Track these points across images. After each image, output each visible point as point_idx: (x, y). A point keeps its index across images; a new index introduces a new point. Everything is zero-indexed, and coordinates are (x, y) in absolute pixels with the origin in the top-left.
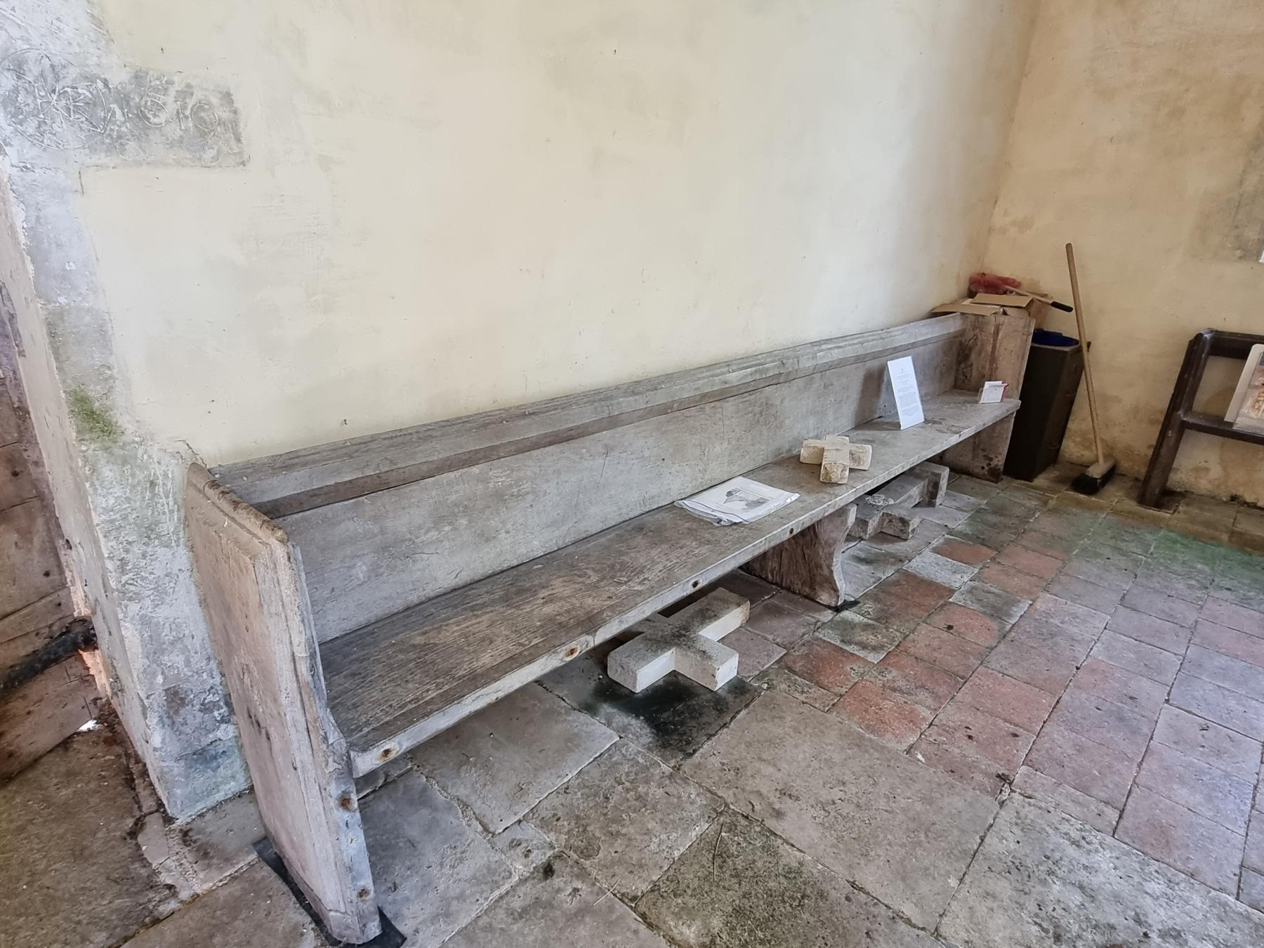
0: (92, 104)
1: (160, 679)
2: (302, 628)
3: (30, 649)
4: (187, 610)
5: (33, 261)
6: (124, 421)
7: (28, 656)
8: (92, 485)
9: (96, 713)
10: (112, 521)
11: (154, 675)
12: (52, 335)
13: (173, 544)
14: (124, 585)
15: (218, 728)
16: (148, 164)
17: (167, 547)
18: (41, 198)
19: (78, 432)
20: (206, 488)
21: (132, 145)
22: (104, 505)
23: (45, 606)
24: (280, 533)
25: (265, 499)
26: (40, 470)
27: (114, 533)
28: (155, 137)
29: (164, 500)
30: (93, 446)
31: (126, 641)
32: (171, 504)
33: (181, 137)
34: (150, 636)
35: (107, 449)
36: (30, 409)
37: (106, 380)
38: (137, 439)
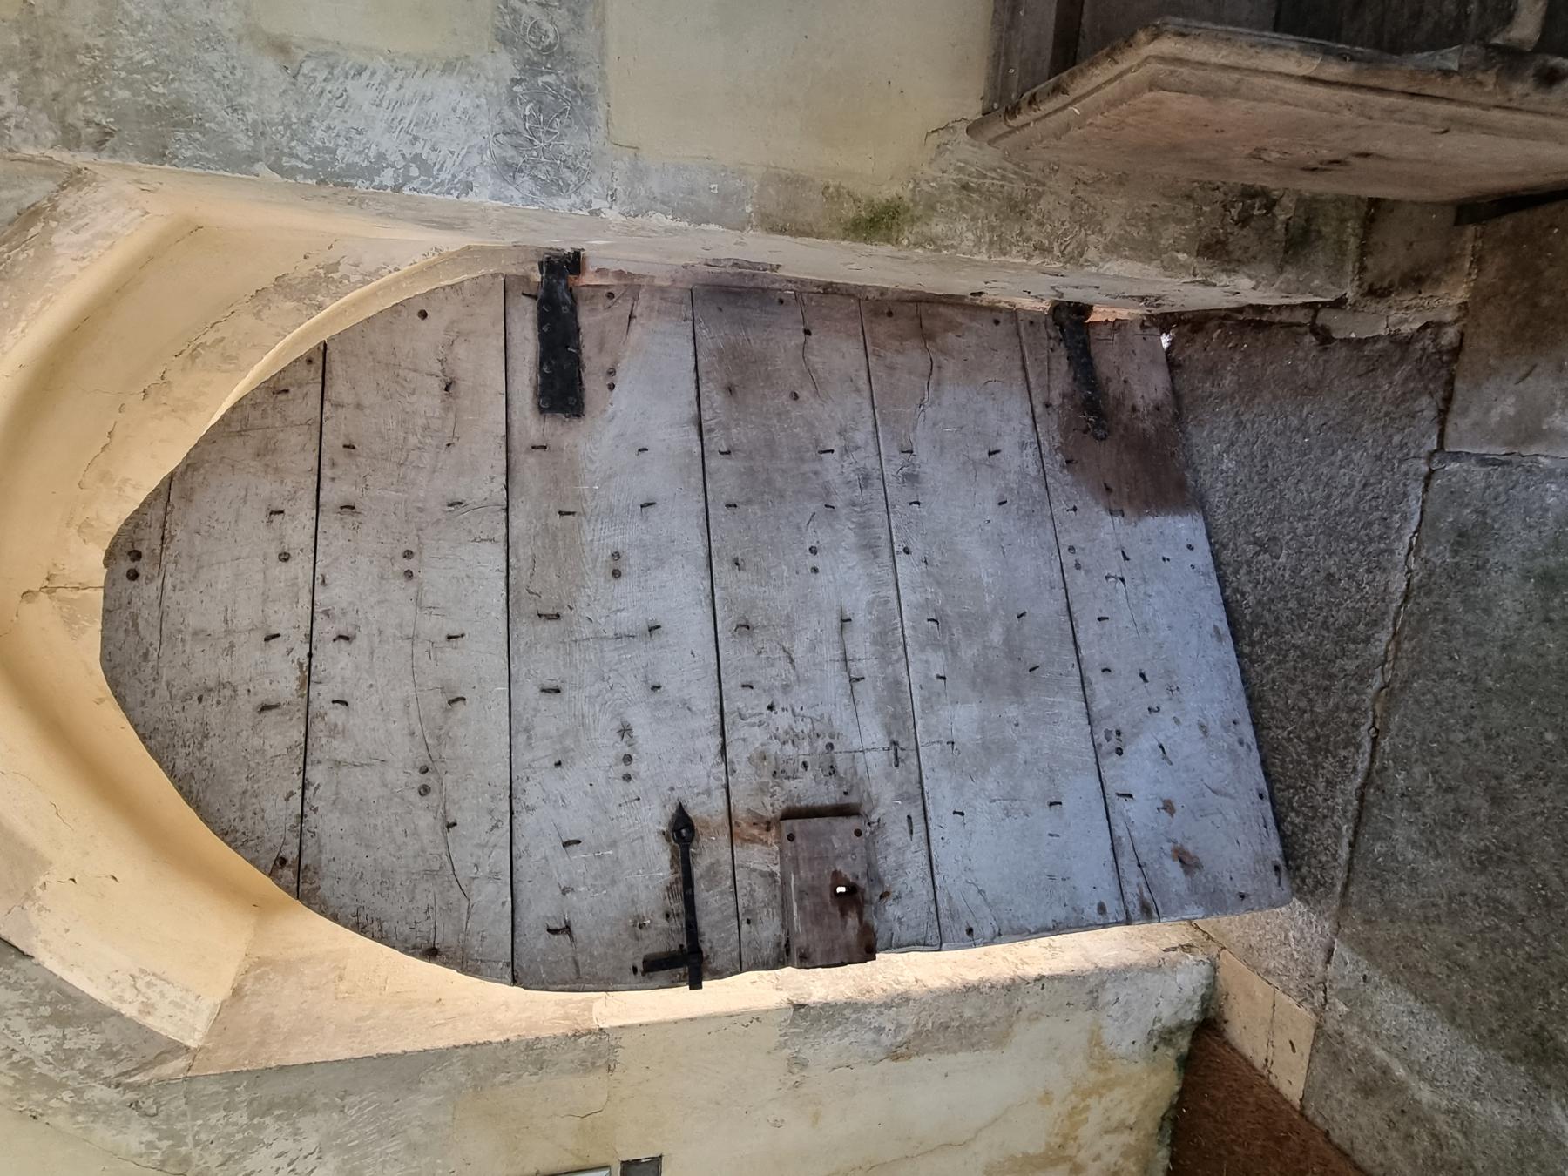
0: (540, 106)
1: (1182, 256)
2: (1281, 52)
3: (1065, 361)
4: (1122, 201)
5: (708, 223)
6: (887, 192)
7: (1069, 365)
8: (946, 247)
9: (1155, 330)
10: (991, 242)
11: (1174, 260)
12: (783, 231)
13: (1040, 189)
14: (1063, 255)
15: (1274, 216)
16: (602, 63)
17: (1040, 197)
18: (643, 193)
19: (888, 241)
20: (1011, 123)
21: (584, 77)
22: (971, 244)
23: (1029, 335)
24: (1141, 36)
25: (1047, 54)
26: (890, 293)
27: (1004, 245)
28: (572, 42)
29: (988, 181)
30: (906, 233)
31: (1122, 273)
32: (994, 175)
33: (568, 10)
34: (1131, 248)
35: (913, 221)
36: (829, 280)
37: (839, 195)
38: (911, 186)
